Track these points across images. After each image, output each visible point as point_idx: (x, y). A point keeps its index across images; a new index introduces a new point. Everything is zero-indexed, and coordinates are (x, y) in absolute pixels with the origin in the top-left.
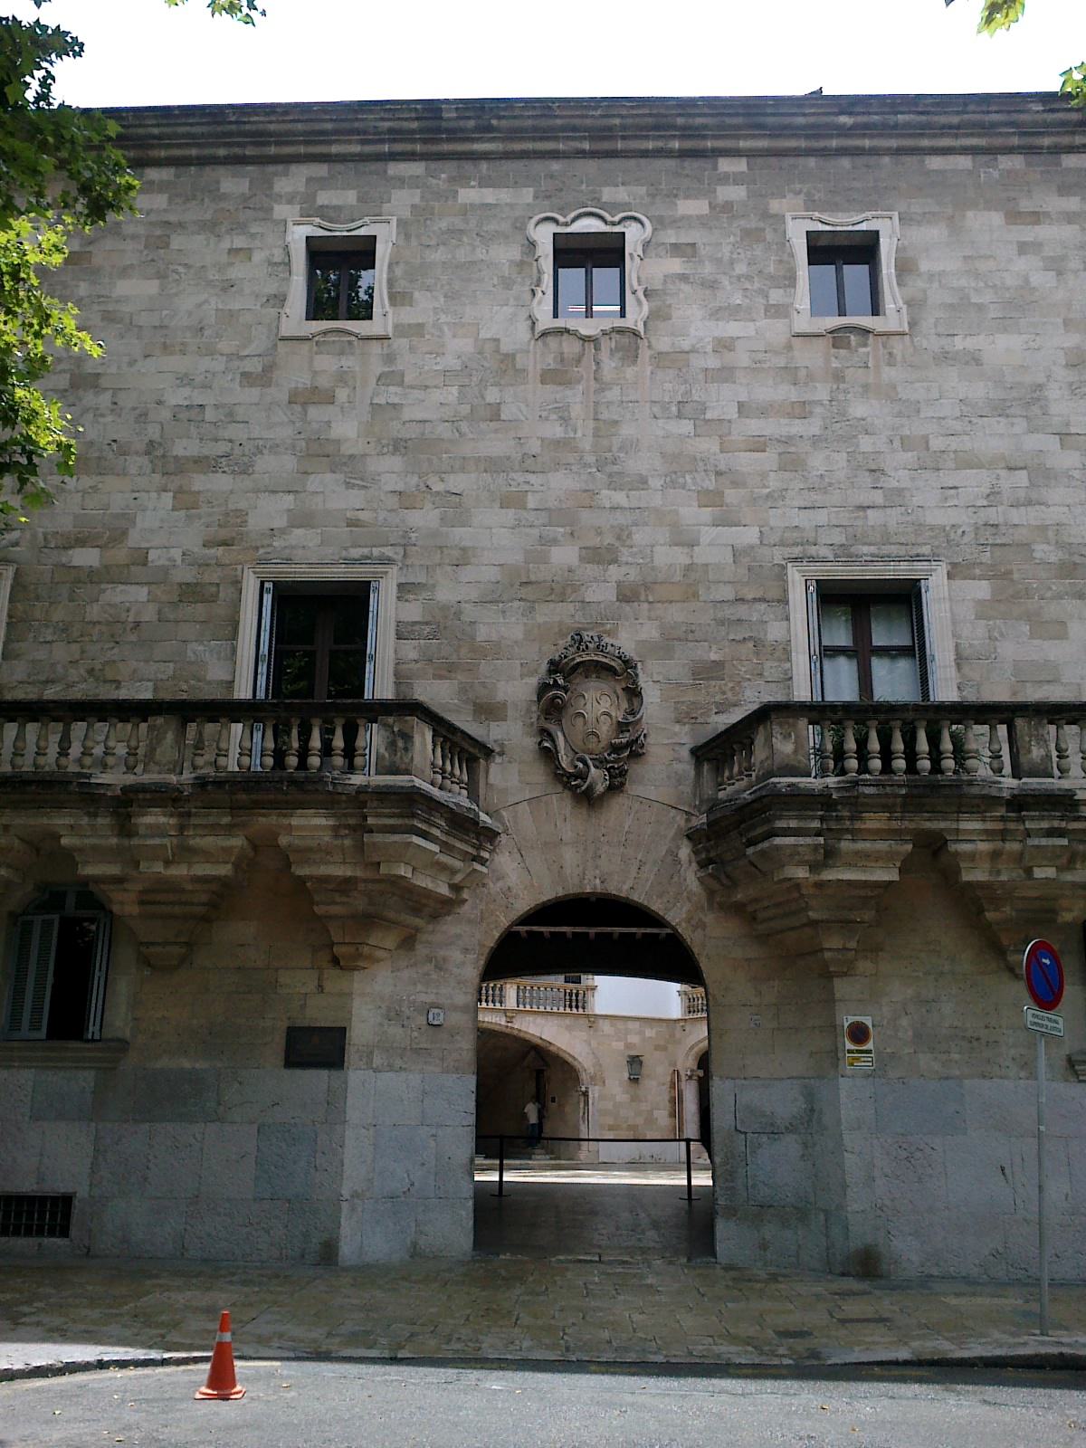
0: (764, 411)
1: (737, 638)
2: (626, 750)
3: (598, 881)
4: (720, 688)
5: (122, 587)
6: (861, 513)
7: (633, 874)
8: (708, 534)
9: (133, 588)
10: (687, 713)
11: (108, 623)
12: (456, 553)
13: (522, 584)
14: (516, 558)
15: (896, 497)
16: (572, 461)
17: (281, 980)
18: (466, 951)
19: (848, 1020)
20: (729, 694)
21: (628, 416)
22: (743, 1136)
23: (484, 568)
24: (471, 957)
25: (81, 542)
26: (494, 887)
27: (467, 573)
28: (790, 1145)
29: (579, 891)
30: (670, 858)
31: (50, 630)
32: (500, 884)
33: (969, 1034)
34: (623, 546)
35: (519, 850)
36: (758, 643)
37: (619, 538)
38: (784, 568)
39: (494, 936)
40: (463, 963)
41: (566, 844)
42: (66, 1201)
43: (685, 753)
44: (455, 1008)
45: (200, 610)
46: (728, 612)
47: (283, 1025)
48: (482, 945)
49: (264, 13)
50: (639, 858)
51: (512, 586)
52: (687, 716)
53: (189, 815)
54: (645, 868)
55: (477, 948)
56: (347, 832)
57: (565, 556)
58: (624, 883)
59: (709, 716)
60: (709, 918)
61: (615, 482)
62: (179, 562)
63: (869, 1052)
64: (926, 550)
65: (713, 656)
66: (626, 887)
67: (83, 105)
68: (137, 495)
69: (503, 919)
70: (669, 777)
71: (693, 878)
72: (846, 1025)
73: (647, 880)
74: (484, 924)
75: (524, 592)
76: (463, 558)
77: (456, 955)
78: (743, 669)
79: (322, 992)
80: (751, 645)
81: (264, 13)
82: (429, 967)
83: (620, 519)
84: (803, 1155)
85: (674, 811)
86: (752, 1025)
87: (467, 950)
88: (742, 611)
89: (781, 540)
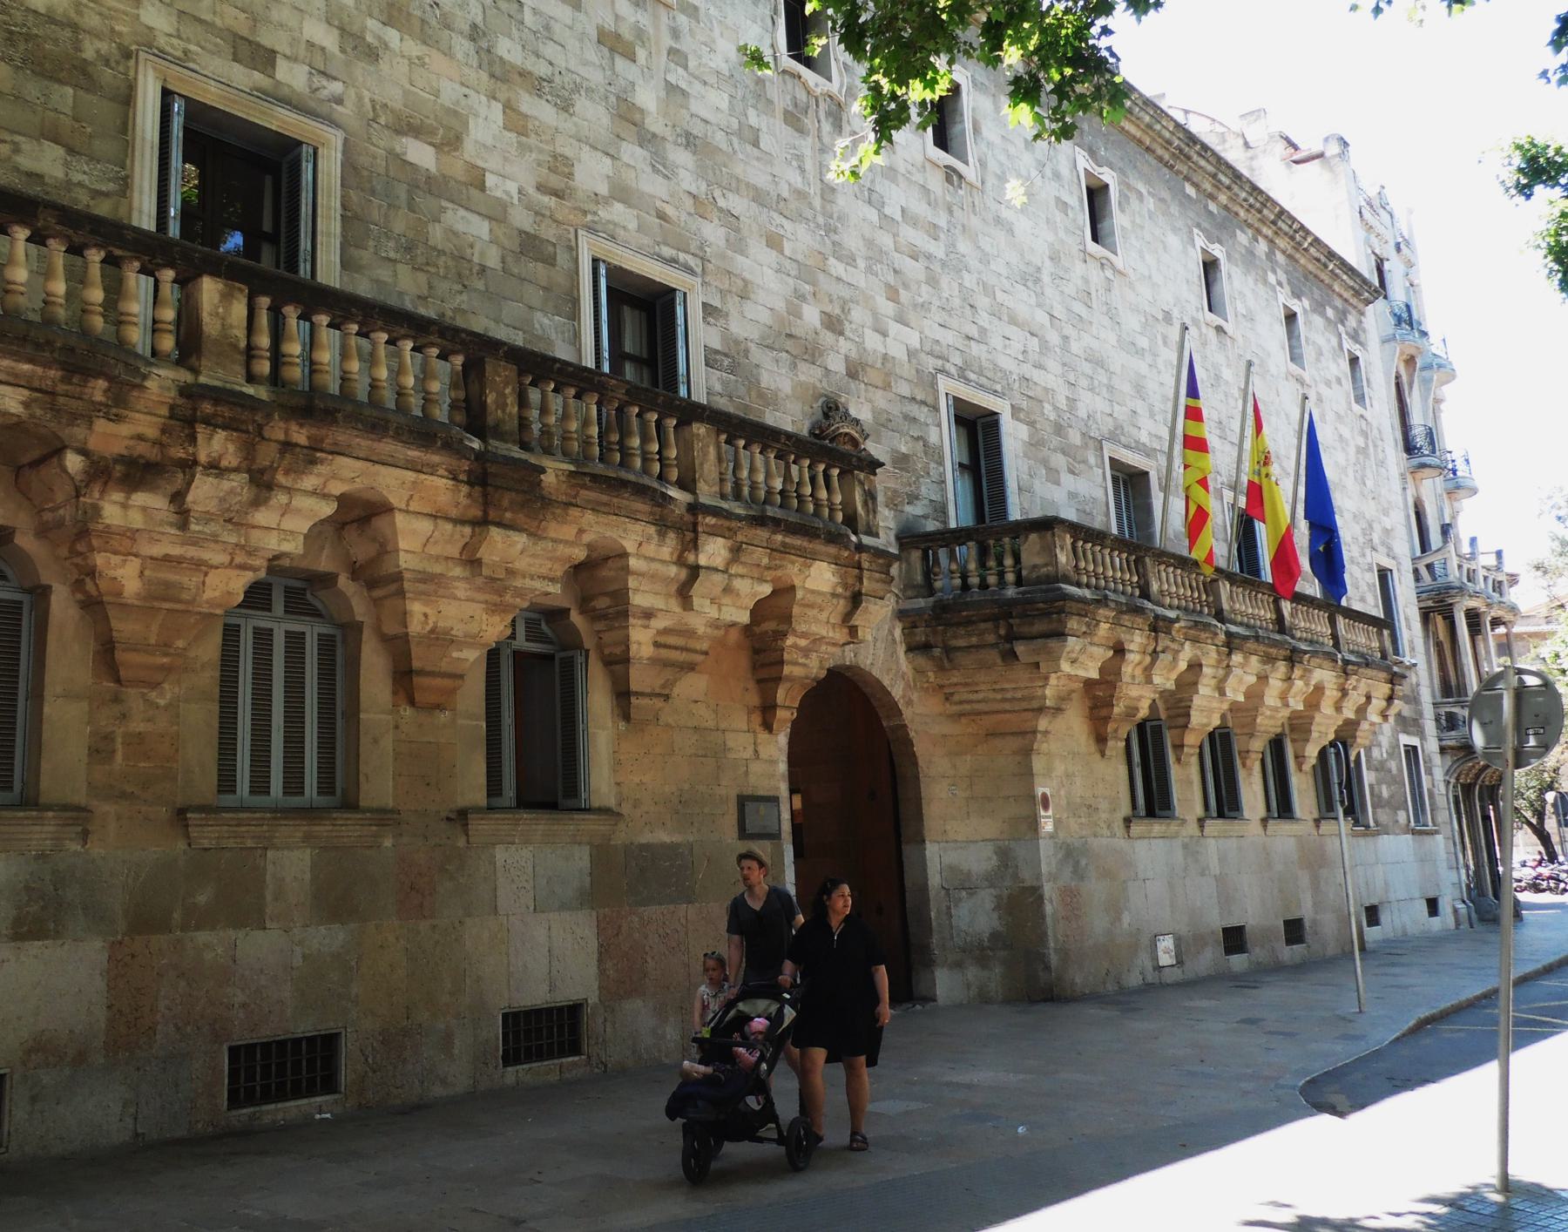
5: (462, 212)
8: (894, 328)
9: (474, 218)
11: (453, 257)
17: (730, 744)
25: (415, 130)
31: (391, 244)
38: (934, 377)
42: (574, 1011)
45: (539, 270)
47: (733, 794)
62: (516, 201)
65: (904, 449)
67: (1337, 1213)
68: (467, 91)
83: (846, 293)
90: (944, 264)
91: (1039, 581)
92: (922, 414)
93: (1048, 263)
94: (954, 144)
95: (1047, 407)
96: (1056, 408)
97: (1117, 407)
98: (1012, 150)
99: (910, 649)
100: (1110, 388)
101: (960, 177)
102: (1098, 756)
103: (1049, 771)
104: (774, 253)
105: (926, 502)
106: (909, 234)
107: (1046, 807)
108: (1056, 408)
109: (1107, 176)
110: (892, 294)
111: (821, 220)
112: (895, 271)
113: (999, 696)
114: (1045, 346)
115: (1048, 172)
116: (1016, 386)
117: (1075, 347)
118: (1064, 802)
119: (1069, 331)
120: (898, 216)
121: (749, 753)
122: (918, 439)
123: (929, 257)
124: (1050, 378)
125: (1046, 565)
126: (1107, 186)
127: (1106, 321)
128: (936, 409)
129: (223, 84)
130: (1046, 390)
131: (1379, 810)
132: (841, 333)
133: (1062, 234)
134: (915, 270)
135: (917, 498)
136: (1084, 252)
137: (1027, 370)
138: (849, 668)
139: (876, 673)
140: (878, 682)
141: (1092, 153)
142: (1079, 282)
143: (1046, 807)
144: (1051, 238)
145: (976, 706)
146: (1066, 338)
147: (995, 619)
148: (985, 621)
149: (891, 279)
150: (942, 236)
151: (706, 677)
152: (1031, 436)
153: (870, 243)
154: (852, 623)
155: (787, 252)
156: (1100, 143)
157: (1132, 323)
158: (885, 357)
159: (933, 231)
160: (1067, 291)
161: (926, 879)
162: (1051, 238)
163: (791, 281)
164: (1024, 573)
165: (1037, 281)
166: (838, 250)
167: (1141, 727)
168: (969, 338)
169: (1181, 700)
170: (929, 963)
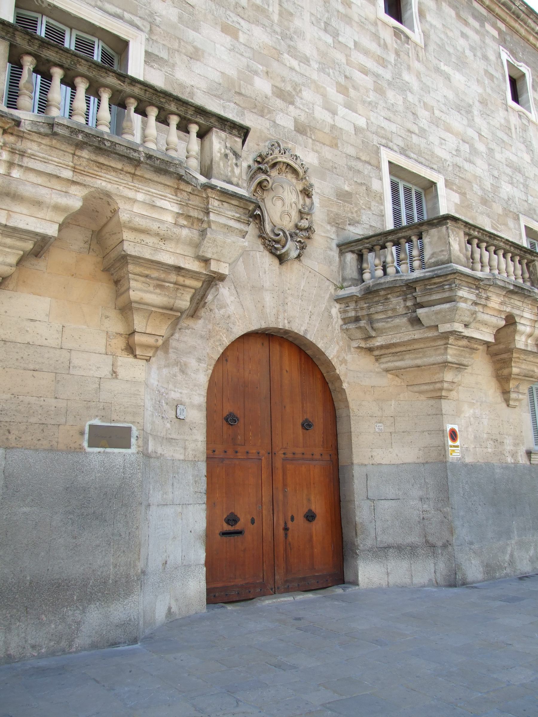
0: (366, 52)
1: (358, 181)
2: (303, 233)
3: (286, 321)
4: (350, 209)
6: (410, 134)
7: (307, 320)
8: (342, 111)
10: (334, 219)
12: (190, 49)
13: (236, 92)
14: (233, 73)
15: (423, 133)
16: (267, 25)
17: (75, 362)
18: (199, 360)
19: (449, 427)
20: (355, 215)
21: (298, 14)
23: (210, 69)
24: (203, 365)
26: (218, 313)
27: (198, 67)
29: (275, 326)
30: (326, 314)
32: (222, 311)
33: (494, 438)
34: (297, 96)
35: (235, 288)
36: (368, 189)
37: (295, 89)
38: (378, 149)
40: (198, 370)
43: (334, 245)
44: (193, 406)
46: (353, 163)
50: (310, 309)
51: (230, 91)
52: (336, 222)
53: (23, 154)
54: (314, 317)
55: (206, 359)
56: (185, 223)
57: (262, 86)
58: (302, 325)
59: (345, 225)
61: (293, 51)
63: (457, 446)
64: (435, 167)
65: (347, 188)
66: (303, 329)
69: (225, 339)
70: (325, 258)
72: (448, 430)
73: (315, 326)
74: (212, 341)
75: (237, 99)
76: (196, 55)
77: (193, 362)
78: (362, 202)
79: (116, 378)
80: (364, 188)
82: (176, 369)
83: (297, 79)
85: (328, 282)
87: (200, 359)
88: (360, 166)
89: (376, 132)
90: (390, 83)
92: (367, 169)
93: (477, 103)
94: (406, 16)
95: (476, 187)
96: (483, 189)
97: (530, 198)
98: (450, 34)
101: (407, 37)
102: (504, 405)
103: (458, 413)
104: (228, 38)
106: (359, 58)
108: (483, 189)
109: (524, 68)
110: (343, 90)
111: (278, 29)
112: (346, 77)
114: (474, 151)
115: (479, 54)
116: (450, 169)
117: (498, 156)
118: (471, 437)
119: (493, 146)
120: (351, 45)
121: (106, 371)
122: (361, 184)
123: (377, 76)
126: (524, 75)
127: (522, 147)
128: (378, 168)
129: (469, 370)
130: (475, 177)
132: (292, 103)
133: (489, 90)
134: (367, 81)
135: (358, 222)
136: (506, 105)
137: (459, 161)
139: (310, 337)
141: (513, 53)
142: (503, 121)
144: (480, 90)
146: (491, 150)
149: (342, 80)
150: (390, 66)
151: (48, 299)
152: (462, 201)
153: (323, 55)
155: (241, 40)
156: (518, 50)
158: (333, 127)
159: (382, 62)
160: (492, 123)
162: (480, 90)
163: (244, 60)
165: (469, 112)
166: (293, 51)
167: (295, 130)
168: (409, 131)
170: (355, 555)
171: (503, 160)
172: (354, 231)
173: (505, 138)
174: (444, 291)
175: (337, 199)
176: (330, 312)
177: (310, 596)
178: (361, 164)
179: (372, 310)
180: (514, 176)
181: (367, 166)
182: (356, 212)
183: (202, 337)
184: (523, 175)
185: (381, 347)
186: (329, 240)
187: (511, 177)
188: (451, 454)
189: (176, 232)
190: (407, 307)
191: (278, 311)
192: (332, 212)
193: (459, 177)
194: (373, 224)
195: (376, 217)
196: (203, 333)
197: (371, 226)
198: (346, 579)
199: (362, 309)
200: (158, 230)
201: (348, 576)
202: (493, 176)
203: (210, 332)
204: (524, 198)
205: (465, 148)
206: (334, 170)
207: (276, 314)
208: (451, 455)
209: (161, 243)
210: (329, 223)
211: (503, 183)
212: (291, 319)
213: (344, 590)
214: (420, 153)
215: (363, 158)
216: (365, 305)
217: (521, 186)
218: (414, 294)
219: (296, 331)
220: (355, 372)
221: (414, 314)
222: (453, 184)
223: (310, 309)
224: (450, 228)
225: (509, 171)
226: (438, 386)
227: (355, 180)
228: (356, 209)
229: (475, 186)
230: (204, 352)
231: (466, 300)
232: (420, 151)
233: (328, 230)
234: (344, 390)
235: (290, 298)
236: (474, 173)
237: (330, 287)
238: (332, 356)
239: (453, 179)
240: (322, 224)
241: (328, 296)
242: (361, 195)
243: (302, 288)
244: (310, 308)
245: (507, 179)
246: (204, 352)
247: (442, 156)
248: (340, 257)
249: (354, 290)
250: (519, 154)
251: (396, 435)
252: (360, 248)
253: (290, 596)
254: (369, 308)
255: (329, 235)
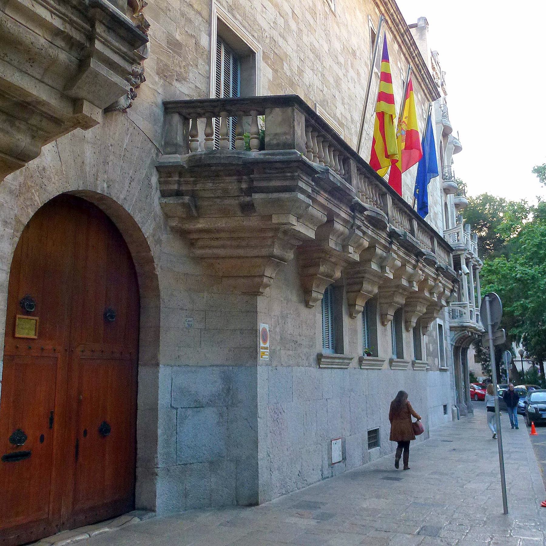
3: (105, 185)
10: (163, 70)
20: (182, 70)
22: (175, 411)
28: (209, 415)
30: (146, 182)
39: (28, 214)
41: (88, 142)
48: (18, 221)
49: (542, 187)
55: (14, 223)
60: (164, 237)
64: (256, 35)
65: (178, 37)
69: (37, 198)
71: (158, 203)
81: (542, 187)
84: (218, 423)
86: (187, 325)
91: (278, 146)
99: (164, 194)
100: (323, 75)
105: (193, 86)
107: (265, 341)
108: (291, 70)
113: (234, 243)
116: (268, 41)
117: (305, 38)
118: (278, 338)
119: (303, 27)
122: (192, 36)
124: (288, 47)
125: (285, 134)
127: (323, 35)
131: (429, 357)
135: (185, 79)
138: (102, 198)
140: (130, 217)
143: (265, 341)
145: (216, 251)
146: (300, 30)
147: (239, 173)
148: (230, 175)
154: (74, 92)
157: (337, 46)
161: (157, 399)
164: (267, 139)
169: (359, 272)
171: (308, 44)
172: (180, 89)
173: (312, 22)
174: (285, 178)
175: (168, 47)
176: (150, 181)
177: (105, 529)
178: (193, 12)
179: (198, 187)
180: (315, 63)
181: (198, 15)
182: (184, 67)
183: (11, 192)
184: (322, 64)
185: (201, 231)
186: (156, 94)
187: (313, 63)
188: (262, 357)
189: (51, 54)
190: (242, 188)
191: (98, 171)
192: (161, 61)
193: (274, 52)
194: (199, 85)
195: (202, 77)
196: (13, 187)
197: (196, 87)
198: (138, 503)
199: (187, 183)
200: (31, 46)
201: (141, 499)
202: (300, 58)
203: (20, 186)
204: (321, 88)
205: (280, 21)
206: (168, 13)
207: (96, 175)
208: (262, 357)
209: (28, 64)
210: (158, 74)
211: (307, 68)
212: (111, 183)
213: (141, 519)
214: (244, 16)
215: (195, 6)
216: (192, 179)
217: (320, 75)
218: (251, 176)
219: (115, 199)
220: (166, 256)
221: (248, 199)
222: (268, 57)
223: (131, 174)
224: (296, 110)
225: (311, 56)
226: (257, 280)
227: (186, 29)
228: (184, 64)
229: (285, 64)
230: (12, 213)
231: (303, 191)
232: (245, 14)
233: (156, 82)
234: (157, 275)
235: (111, 157)
236: (285, 51)
237: (153, 151)
238: (148, 234)
239: (269, 53)
240: (151, 73)
241: (148, 162)
242: (190, 48)
243: (125, 146)
244: (131, 172)
245: (310, 64)
246: (12, 213)
247: (262, 25)
248: (165, 117)
249: (179, 158)
250: (320, 41)
251: (206, 332)
252: (183, 111)
253: (82, 533)
254: (195, 183)
255: (156, 88)
